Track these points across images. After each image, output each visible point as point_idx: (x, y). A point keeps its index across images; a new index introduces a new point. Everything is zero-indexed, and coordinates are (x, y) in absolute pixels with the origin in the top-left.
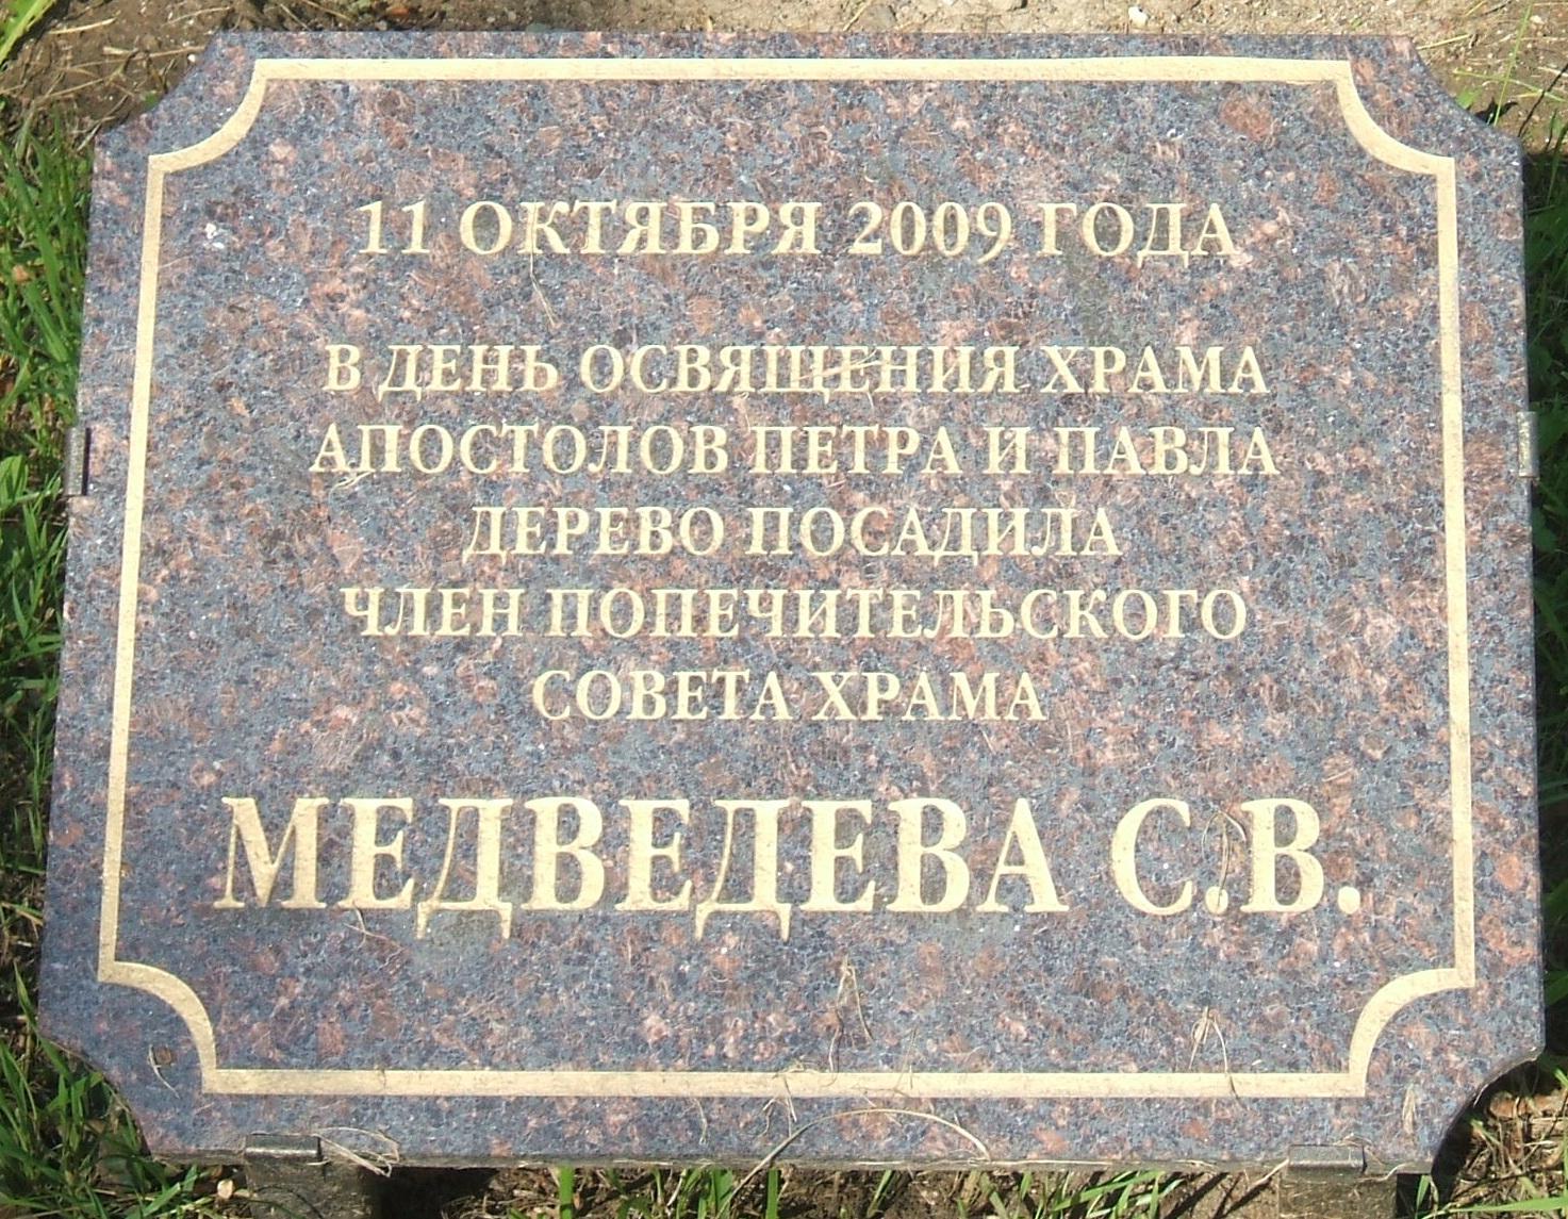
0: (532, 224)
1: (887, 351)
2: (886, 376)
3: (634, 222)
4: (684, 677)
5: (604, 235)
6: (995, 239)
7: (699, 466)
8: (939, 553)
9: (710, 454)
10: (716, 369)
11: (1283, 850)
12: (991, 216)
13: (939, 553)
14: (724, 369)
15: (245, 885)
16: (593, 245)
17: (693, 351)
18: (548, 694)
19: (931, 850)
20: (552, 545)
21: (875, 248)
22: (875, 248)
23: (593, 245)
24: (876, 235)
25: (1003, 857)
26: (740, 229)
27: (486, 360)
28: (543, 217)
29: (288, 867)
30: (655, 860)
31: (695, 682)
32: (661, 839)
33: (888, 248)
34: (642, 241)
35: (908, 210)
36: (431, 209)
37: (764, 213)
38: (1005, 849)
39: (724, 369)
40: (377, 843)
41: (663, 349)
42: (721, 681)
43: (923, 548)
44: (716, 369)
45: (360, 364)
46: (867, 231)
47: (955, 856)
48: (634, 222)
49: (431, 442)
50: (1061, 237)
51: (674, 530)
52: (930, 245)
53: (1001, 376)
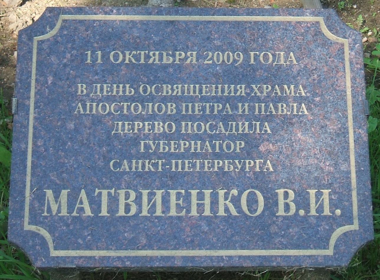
0: (127, 56)
1: (214, 86)
2: (214, 92)
3: (152, 56)
4: (187, 162)
5: (145, 59)
6: (239, 61)
7: (169, 112)
8: (227, 133)
9: (282, 110)
10: (173, 90)
11: (126, 201)
12: (238, 55)
13: (227, 133)
14: (238, 90)
15: (49, 210)
16: (142, 61)
17: (267, 86)
18: (113, 165)
19: (286, 201)
20: (133, 131)
21: (211, 62)
22: (211, 62)
23: (142, 61)
24: (209, 60)
25: (78, 203)
26: (178, 57)
27: (216, 88)
28: (130, 54)
29: (59, 207)
30: (177, 204)
31: (189, 163)
32: (178, 199)
33: (214, 62)
34: (154, 60)
35: (218, 54)
36: (91, 52)
37: (183, 54)
38: (79, 201)
39: (238, 90)
40: (176, 201)
41: (160, 85)
42: (196, 162)
43: (224, 131)
44: (173, 90)
45: (86, 89)
46: (209, 58)
47: (133, 203)
48: (152, 56)
49: (104, 107)
50: (255, 59)
51: (163, 127)
52: (223, 61)
53: (178, 91)
